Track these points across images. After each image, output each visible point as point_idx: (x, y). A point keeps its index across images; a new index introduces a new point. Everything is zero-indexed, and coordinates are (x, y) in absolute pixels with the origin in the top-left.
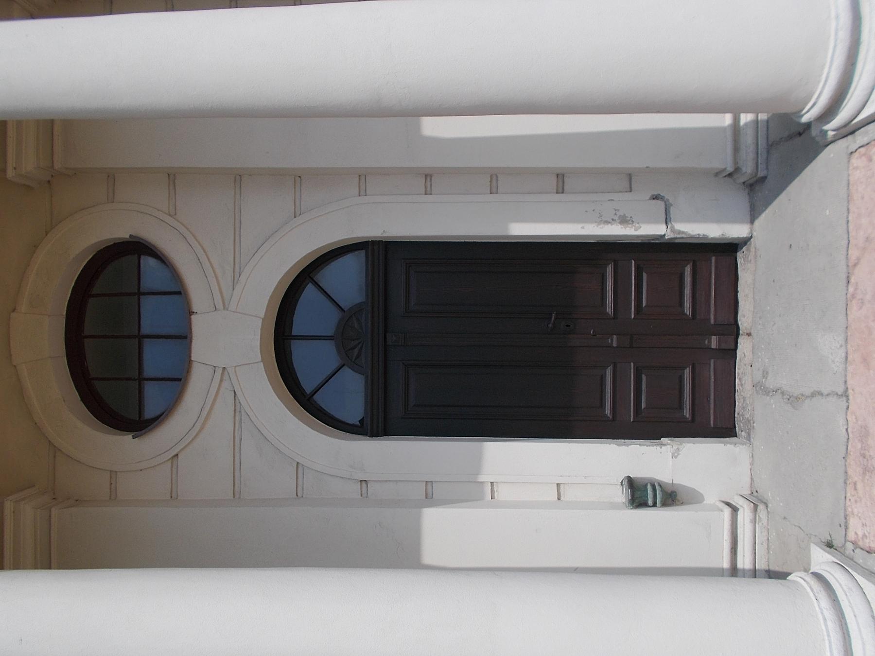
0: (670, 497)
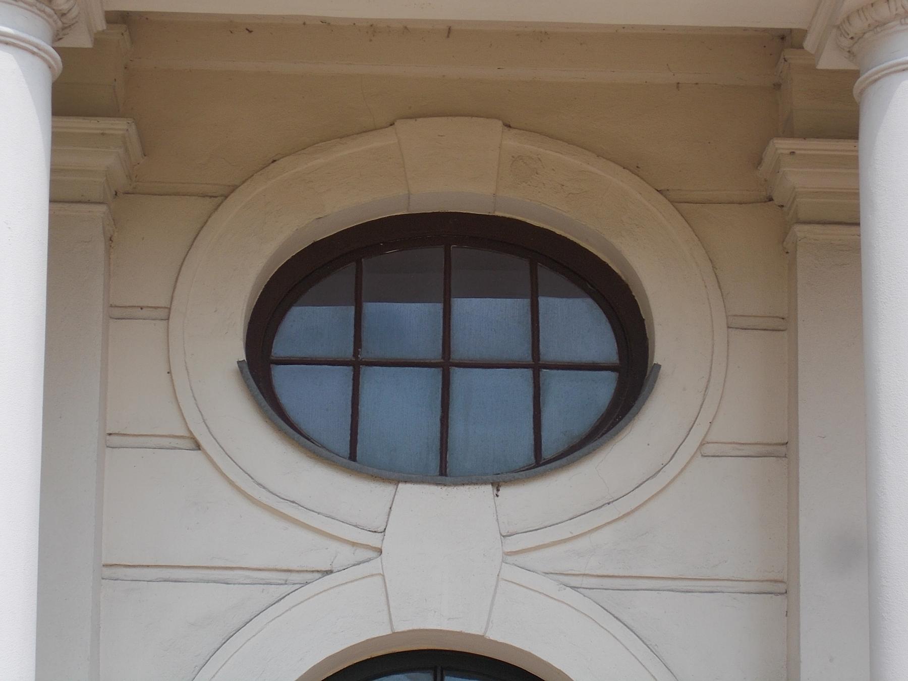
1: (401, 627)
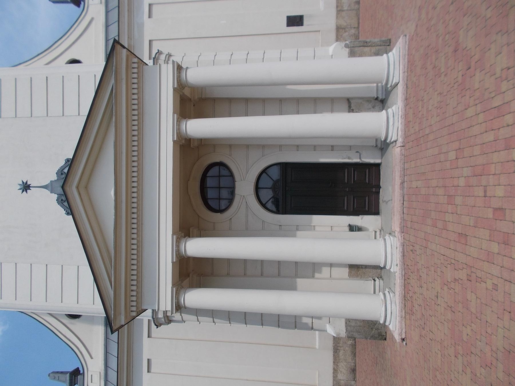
0: (359, 229)
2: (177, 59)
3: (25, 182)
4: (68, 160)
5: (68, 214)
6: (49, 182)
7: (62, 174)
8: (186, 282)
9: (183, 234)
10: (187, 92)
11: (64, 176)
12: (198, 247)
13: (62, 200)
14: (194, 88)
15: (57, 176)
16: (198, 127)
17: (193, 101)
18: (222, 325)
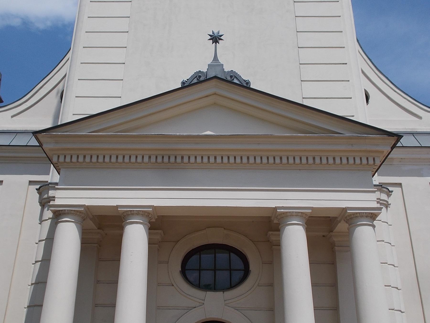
1: (207, 317)
2: (384, 215)
3: (222, 38)
4: (248, 83)
5: (183, 83)
6: (222, 63)
7: (231, 77)
8: (91, 225)
9: (154, 220)
10: (342, 226)
11: (229, 79)
12: (136, 241)
13: (200, 77)
14: (348, 235)
15: (228, 72)
16: (295, 242)
17: (331, 238)
18: (30, 273)
